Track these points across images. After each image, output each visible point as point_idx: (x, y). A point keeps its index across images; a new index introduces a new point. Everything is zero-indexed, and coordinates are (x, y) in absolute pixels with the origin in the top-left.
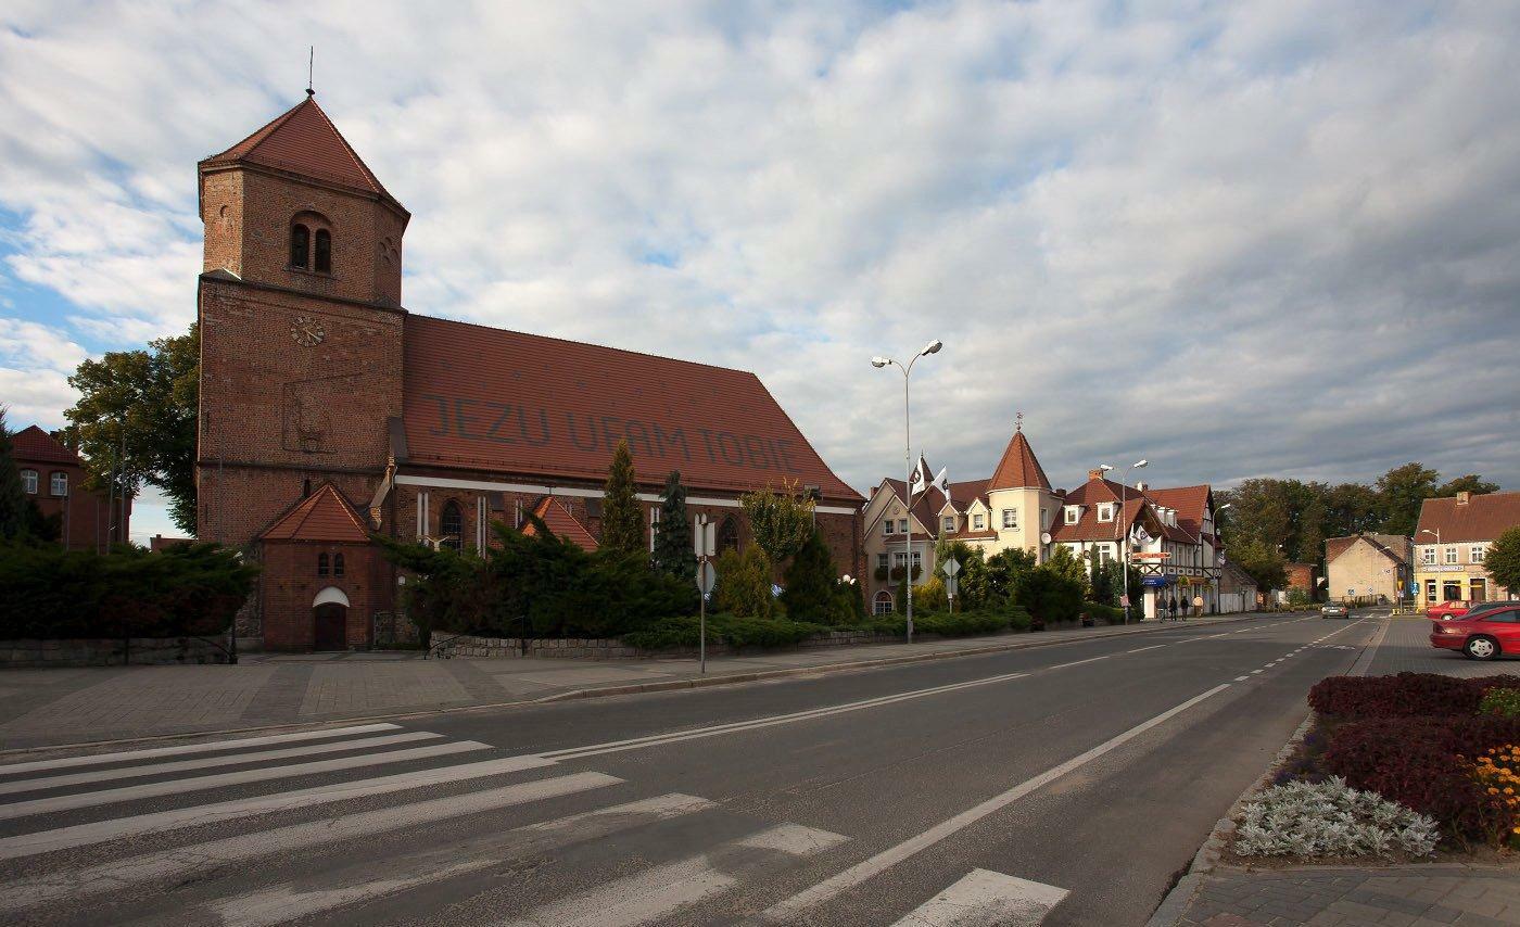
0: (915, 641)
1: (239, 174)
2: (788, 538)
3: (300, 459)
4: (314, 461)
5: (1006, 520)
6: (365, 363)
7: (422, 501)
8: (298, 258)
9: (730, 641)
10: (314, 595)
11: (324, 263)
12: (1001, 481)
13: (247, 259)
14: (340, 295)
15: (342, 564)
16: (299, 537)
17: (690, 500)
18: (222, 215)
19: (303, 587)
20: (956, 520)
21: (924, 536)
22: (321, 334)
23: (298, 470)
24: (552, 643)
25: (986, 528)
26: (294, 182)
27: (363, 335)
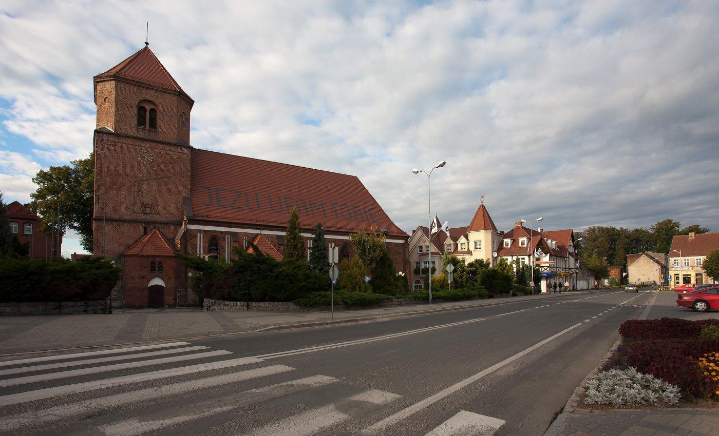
0: (433, 303)
1: (113, 82)
2: (373, 254)
3: (142, 217)
4: (149, 218)
5: (476, 246)
6: (173, 171)
7: (200, 237)
8: (141, 122)
9: (345, 303)
10: (149, 281)
11: (153, 124)
12: (473, 227)
13: (117, 123)
14: (161, 139)
15: (162, 266)
16: (141, 254)
17: (326, 236)
18: (105, 102)
19: (143, 277)
20: (452, 246)
21: (437, 254)
22: (152, 158)
23: (141, 222)
24: (261, 304)
25: (466, 249)
26: (139, 86)
27: (172, 158)
